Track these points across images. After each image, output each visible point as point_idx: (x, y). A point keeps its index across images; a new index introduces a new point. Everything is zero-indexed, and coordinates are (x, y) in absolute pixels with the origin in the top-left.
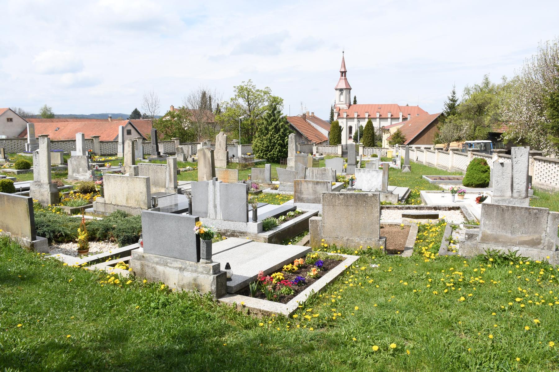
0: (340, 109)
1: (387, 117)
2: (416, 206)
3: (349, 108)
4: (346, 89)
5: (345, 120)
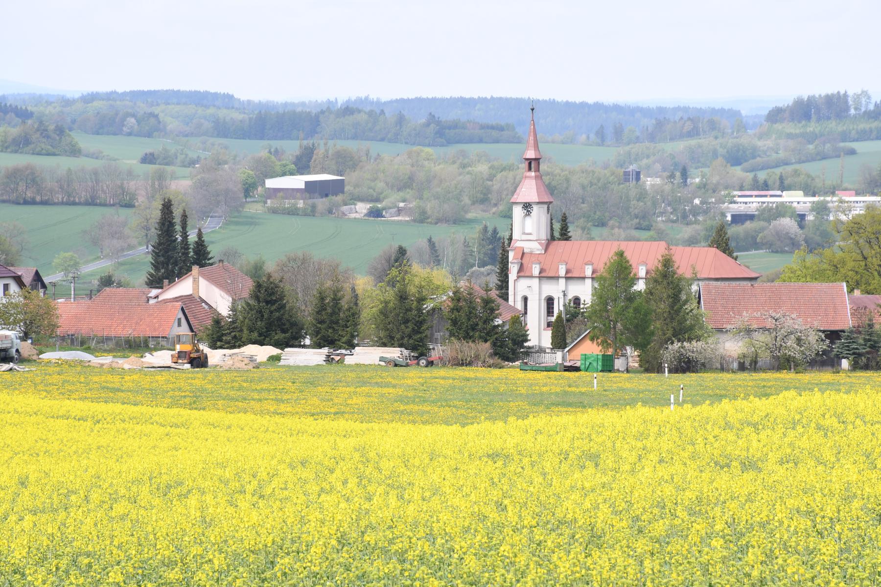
0: (523, 254)
1: (557, 275)
2: (385, 390)
3: (546, 250)
4: (539, 203)
5: (537, 280)
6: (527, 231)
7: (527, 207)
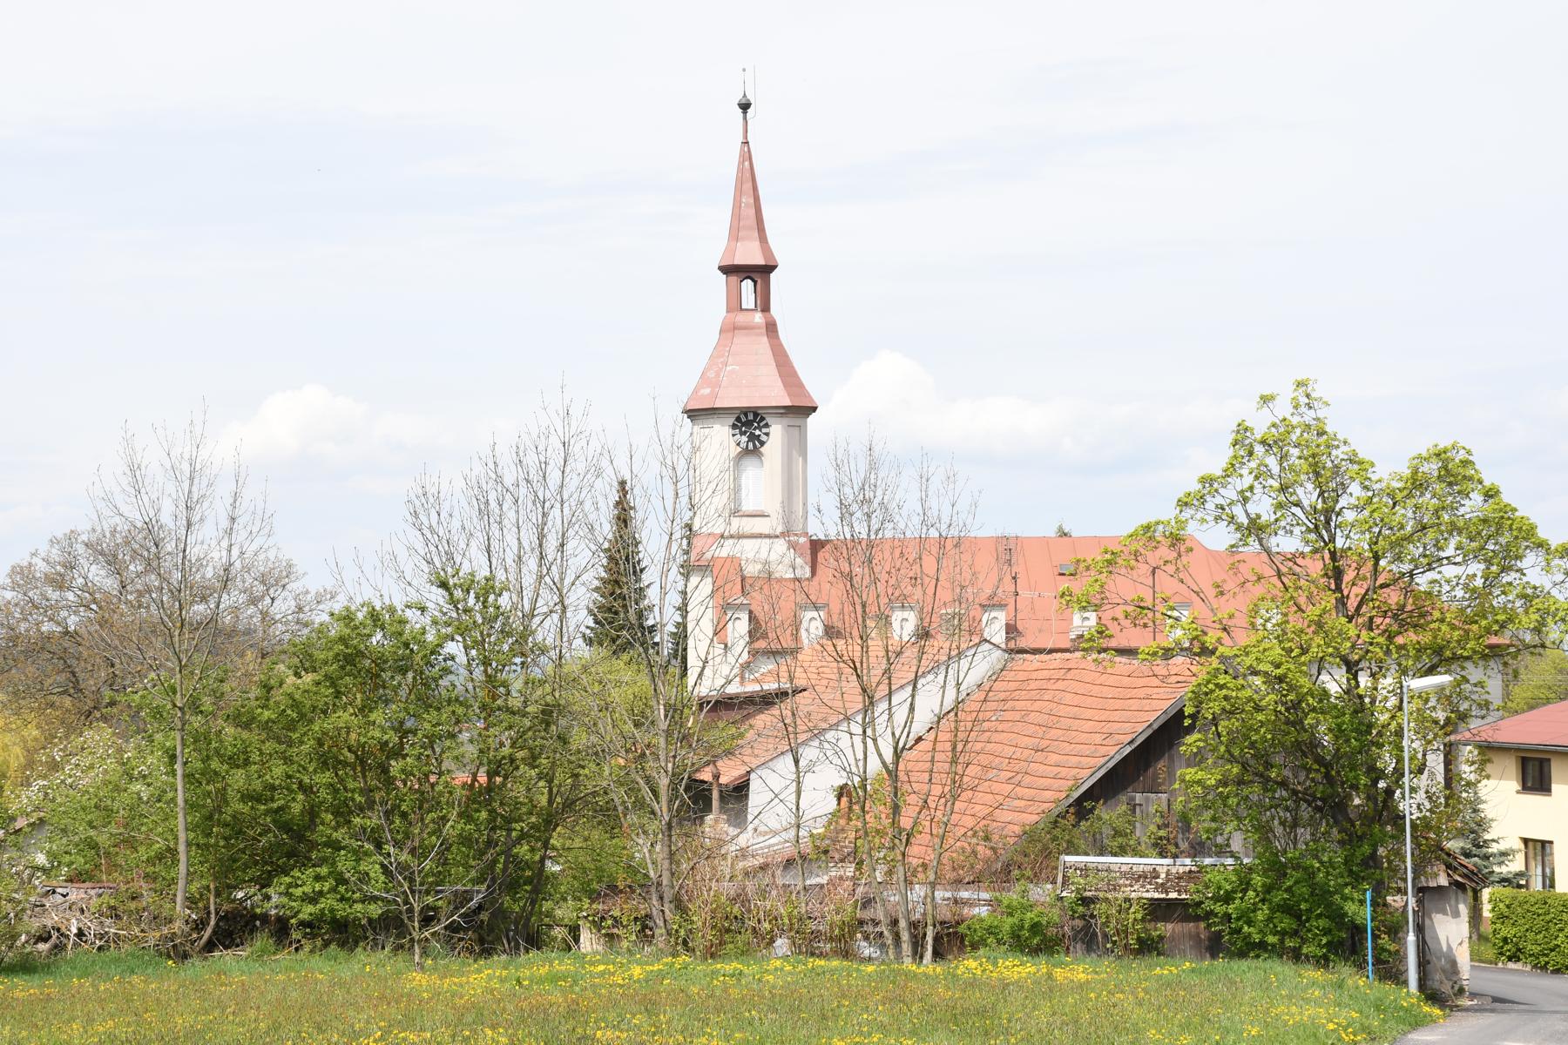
6: (747, 507)
7: (748, 424)
